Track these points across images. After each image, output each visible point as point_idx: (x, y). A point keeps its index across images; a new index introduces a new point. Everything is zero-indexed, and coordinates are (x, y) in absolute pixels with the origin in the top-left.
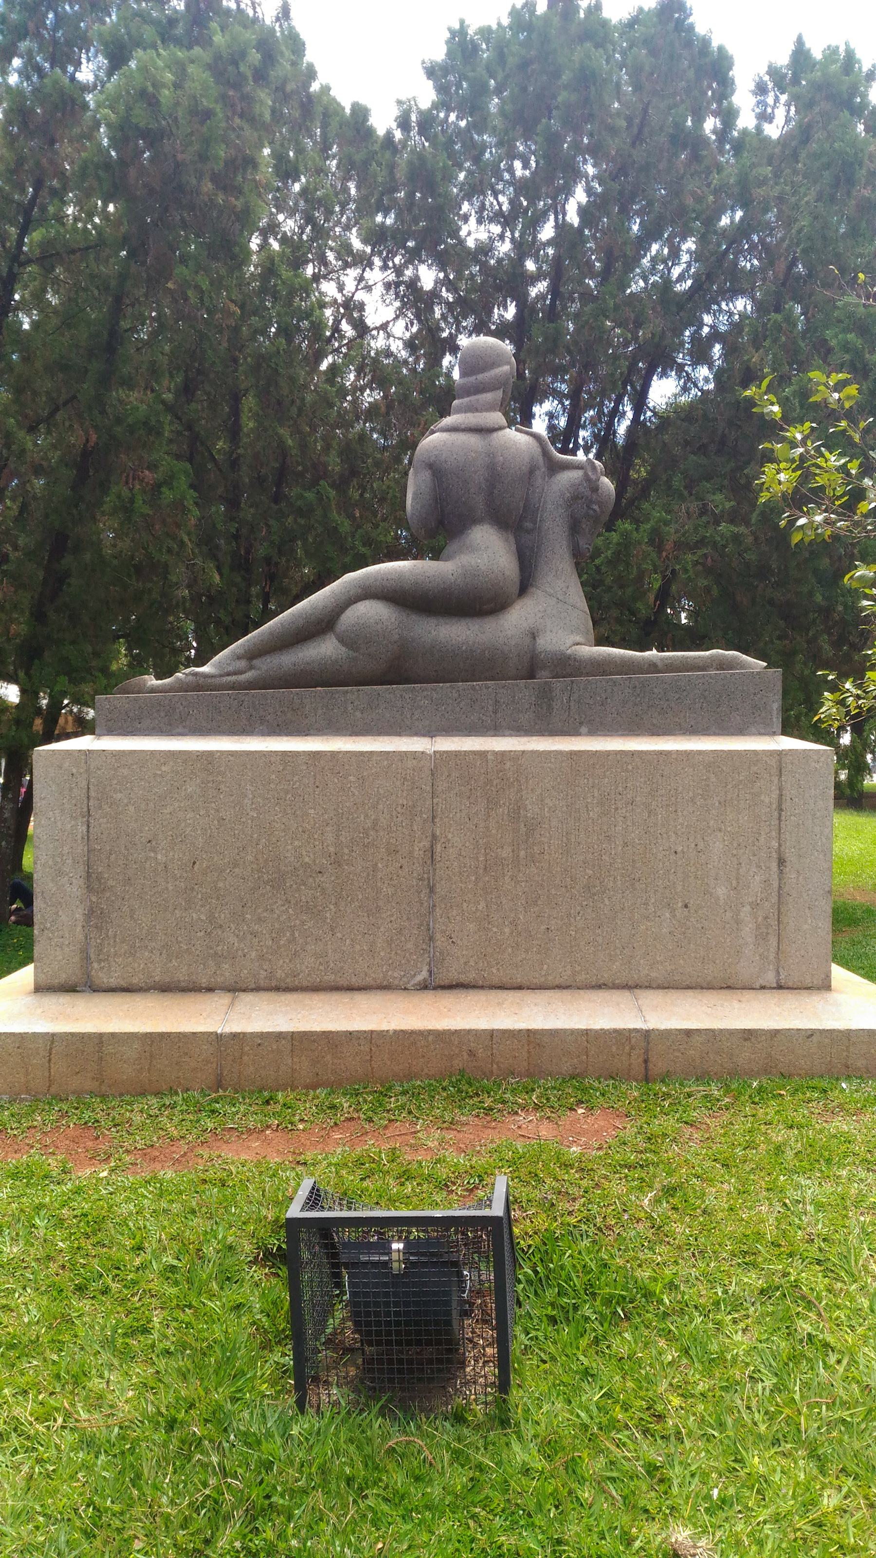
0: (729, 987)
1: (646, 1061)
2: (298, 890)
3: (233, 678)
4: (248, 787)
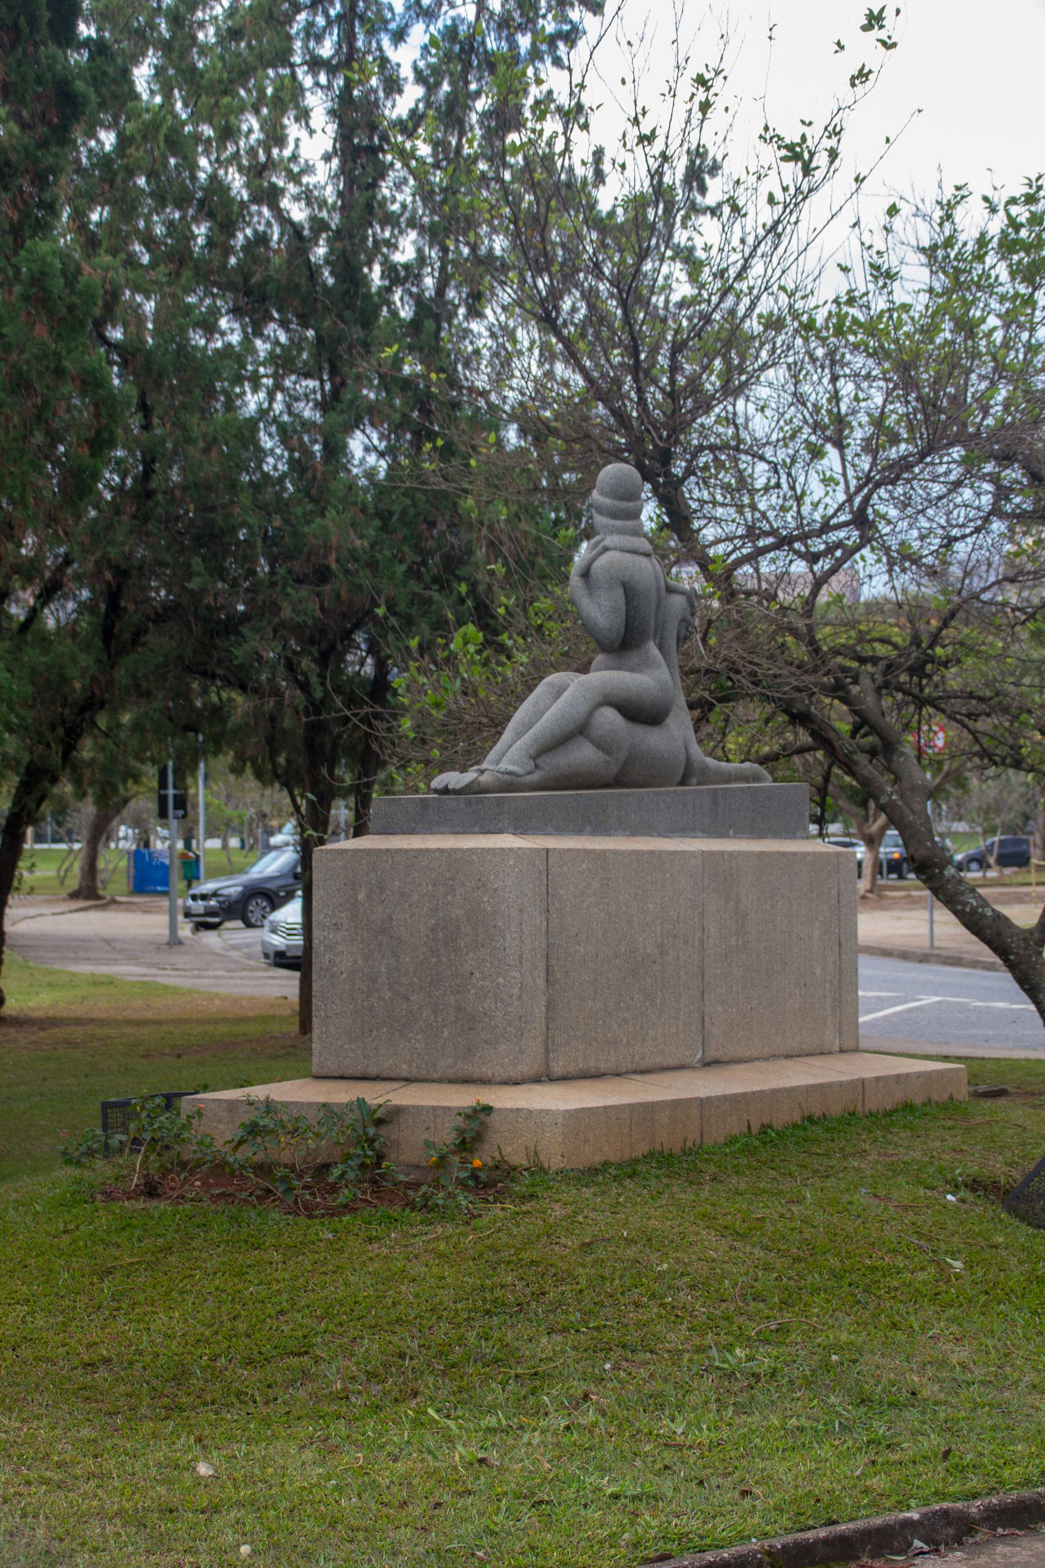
0: (822, 1054)
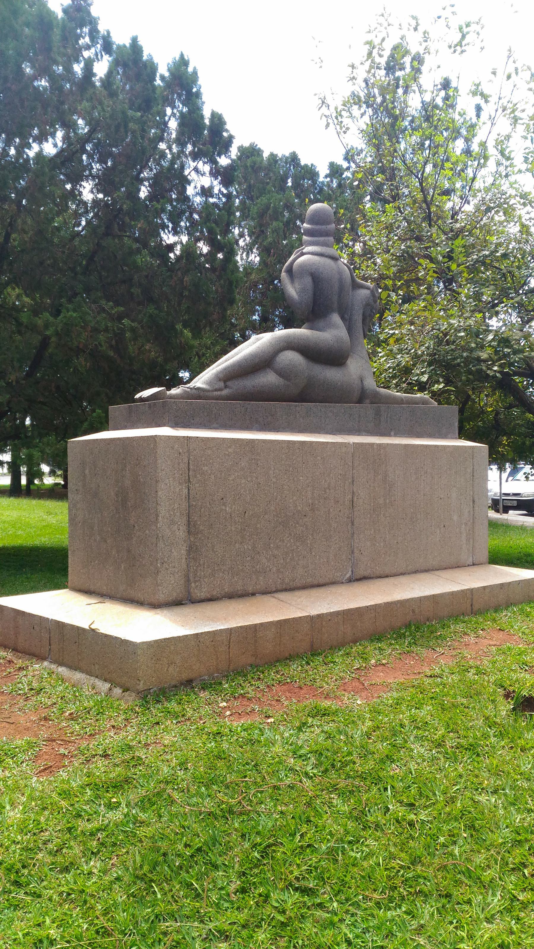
0: (458, 567)
1: (471, 605)
2: (295, 527)
3: (219, 393)
4: (272, 463)
